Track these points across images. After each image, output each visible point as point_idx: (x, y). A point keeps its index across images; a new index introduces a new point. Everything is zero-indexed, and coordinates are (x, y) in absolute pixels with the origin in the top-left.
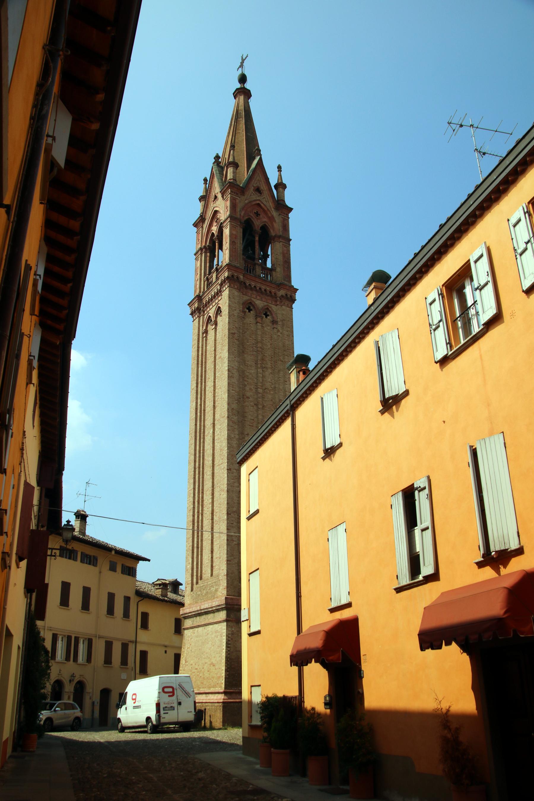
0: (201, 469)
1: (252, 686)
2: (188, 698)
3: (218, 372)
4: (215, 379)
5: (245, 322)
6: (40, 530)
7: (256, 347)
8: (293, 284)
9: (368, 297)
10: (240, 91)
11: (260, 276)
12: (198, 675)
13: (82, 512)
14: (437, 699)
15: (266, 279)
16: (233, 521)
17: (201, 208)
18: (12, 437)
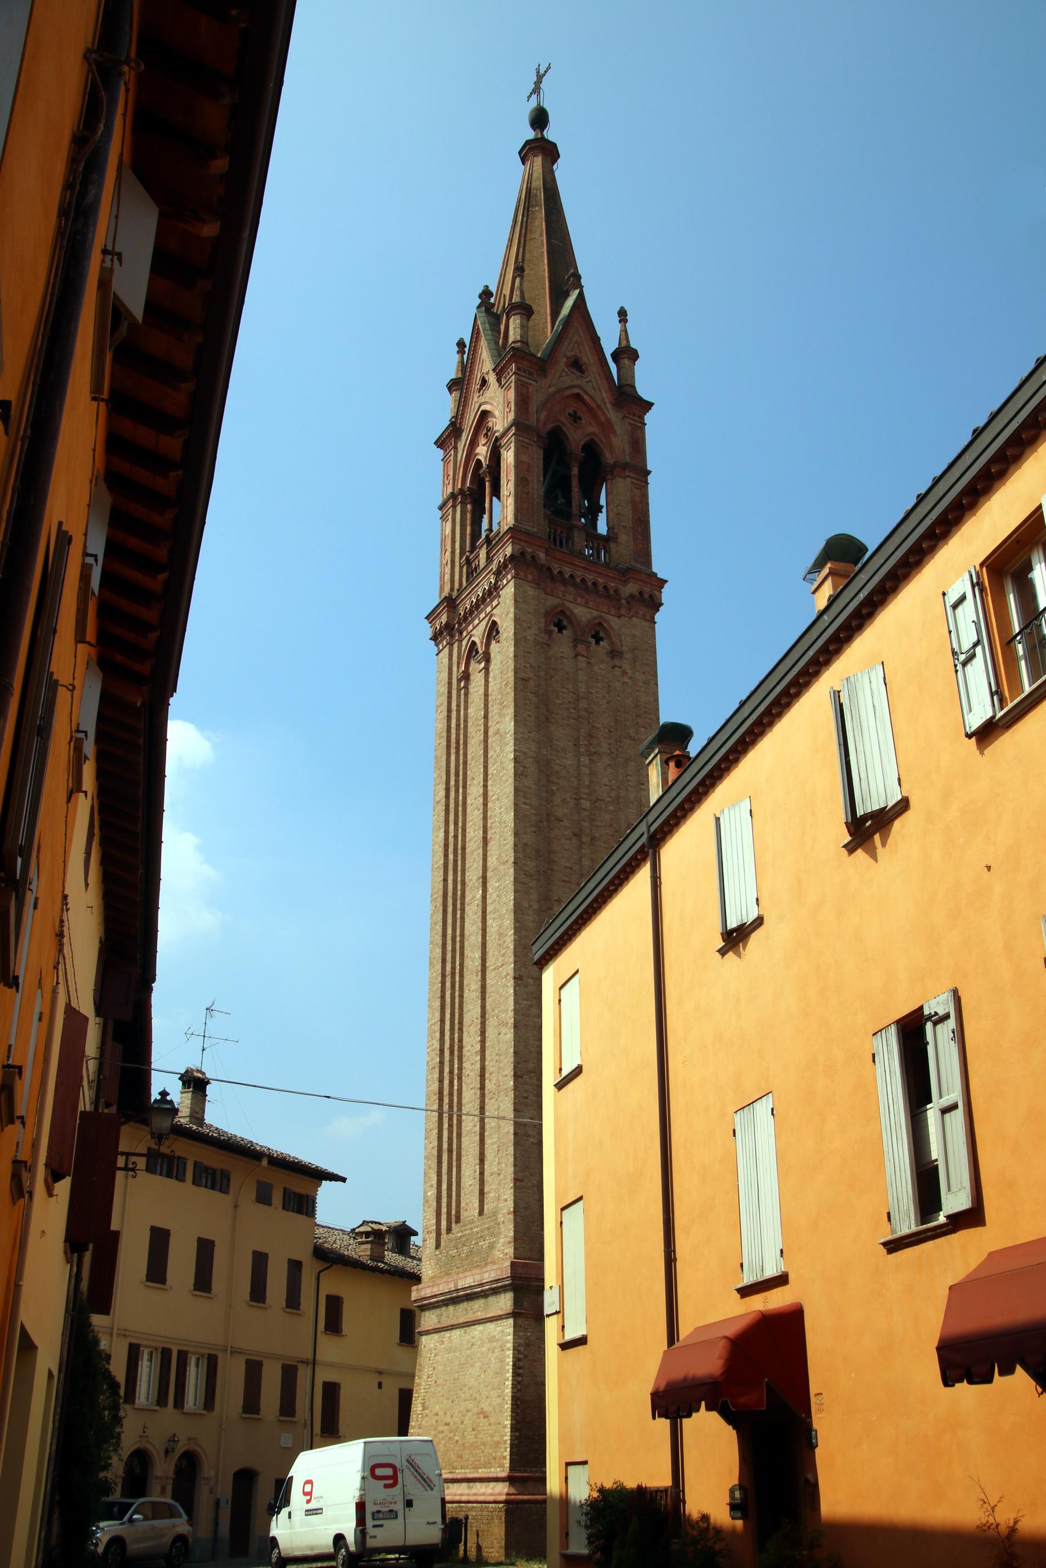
0: (457, 979)
1: (568, 1464)
2: (427, 1490)
3: (494, 765)
4: (486, 780)
5: (550, 654)
6: (103, 1113)
7: (574, 709)
8: (655, 569)
9: (817, 594)
10: (533, 145)
11: (582, 554)
12: (450, 1438)
13: (196, 1074)
14: (985, 1502)
15: (596, 560)
16: (526, 1091)
17: (452, 406)
18: (35, 907)
